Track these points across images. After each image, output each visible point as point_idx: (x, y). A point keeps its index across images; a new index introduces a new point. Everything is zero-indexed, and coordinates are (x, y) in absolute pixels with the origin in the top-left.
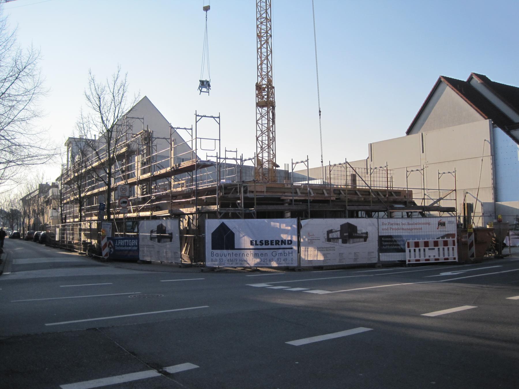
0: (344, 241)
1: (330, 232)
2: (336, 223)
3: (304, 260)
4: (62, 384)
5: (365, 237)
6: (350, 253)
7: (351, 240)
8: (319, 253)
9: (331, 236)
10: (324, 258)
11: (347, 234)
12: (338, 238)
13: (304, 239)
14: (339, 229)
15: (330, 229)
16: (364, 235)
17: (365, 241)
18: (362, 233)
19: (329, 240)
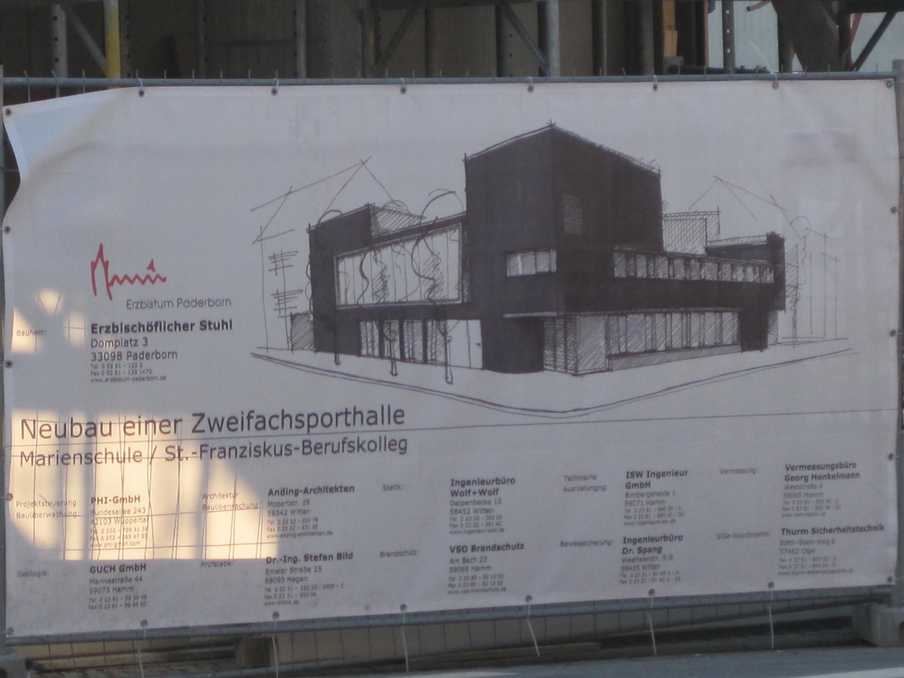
0: (516, 345)
1: (343, 236)
2: (414, 139)
3: (47, 566)
4: (558, 256)
5: (746, 294)
6: (579, 483)
7: (592, 332)
8: (222, 481)
9: (355, 281)
10: (285, 533)
11: (546, 262)
12: (436, 313)
13: (41, 326)
14: (457, 205)
15: (349, 204)
16: (745, 275)
17: (753, 336)
18: (719, 254)
19: (334, 327)
